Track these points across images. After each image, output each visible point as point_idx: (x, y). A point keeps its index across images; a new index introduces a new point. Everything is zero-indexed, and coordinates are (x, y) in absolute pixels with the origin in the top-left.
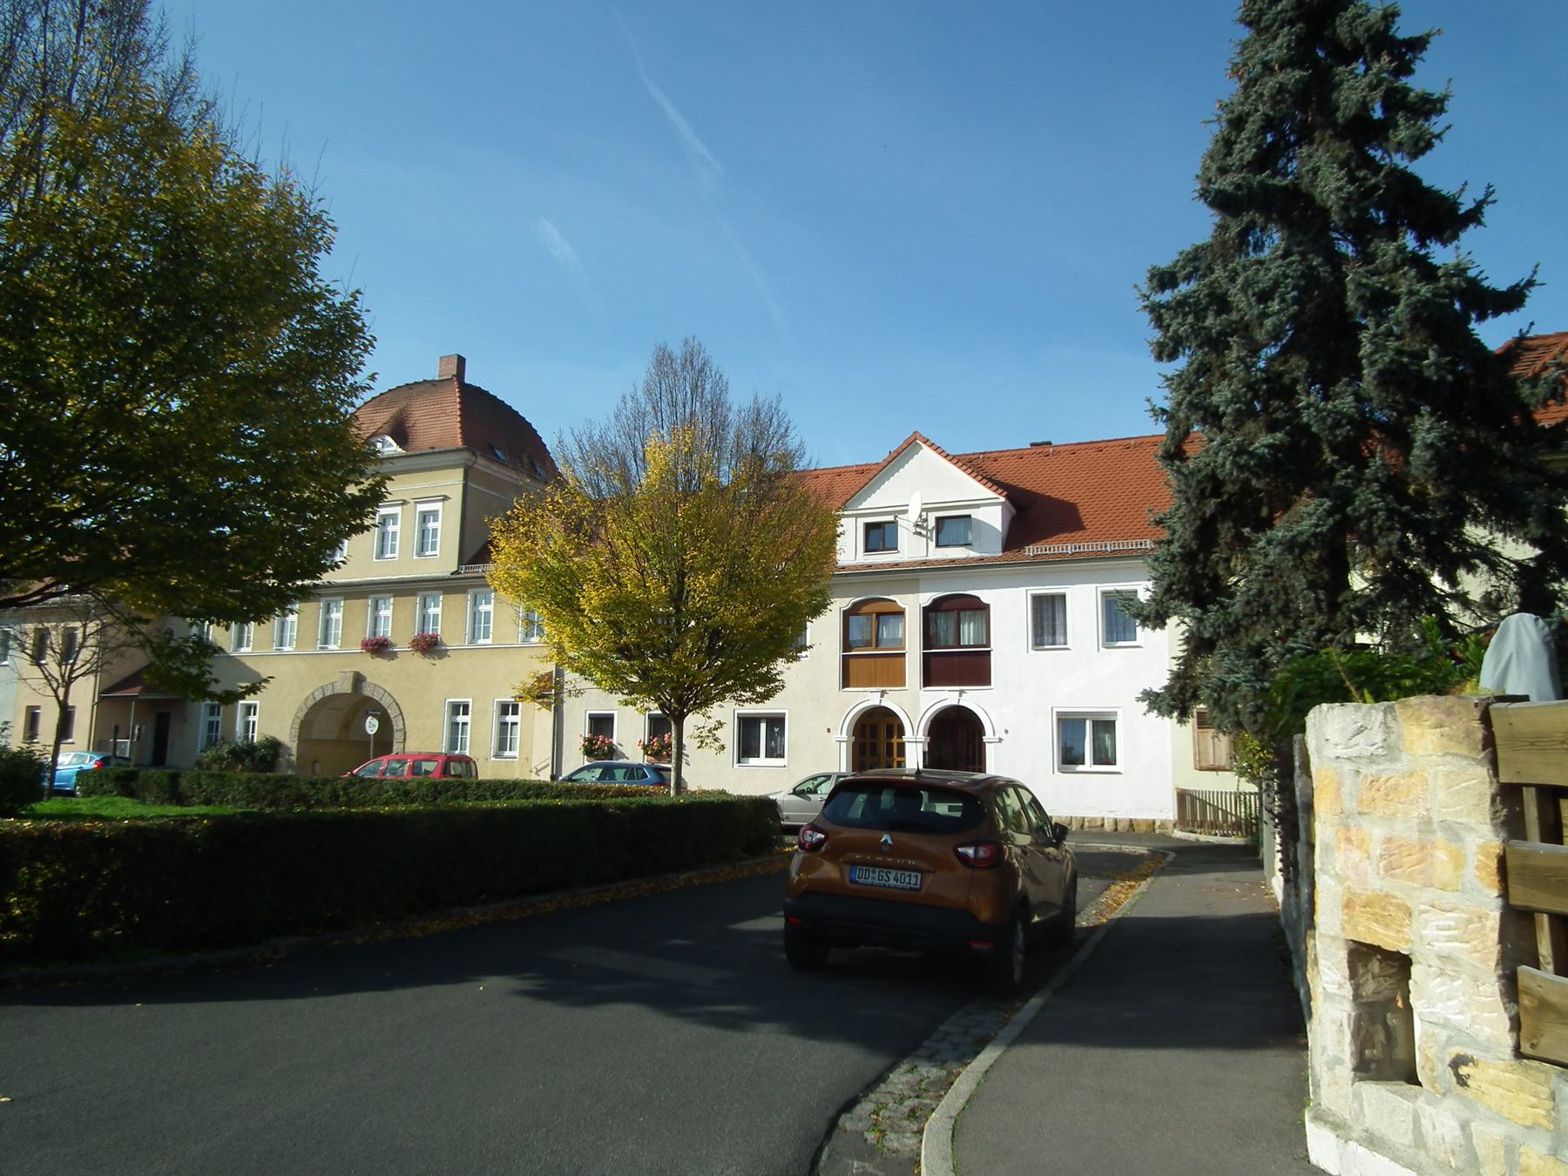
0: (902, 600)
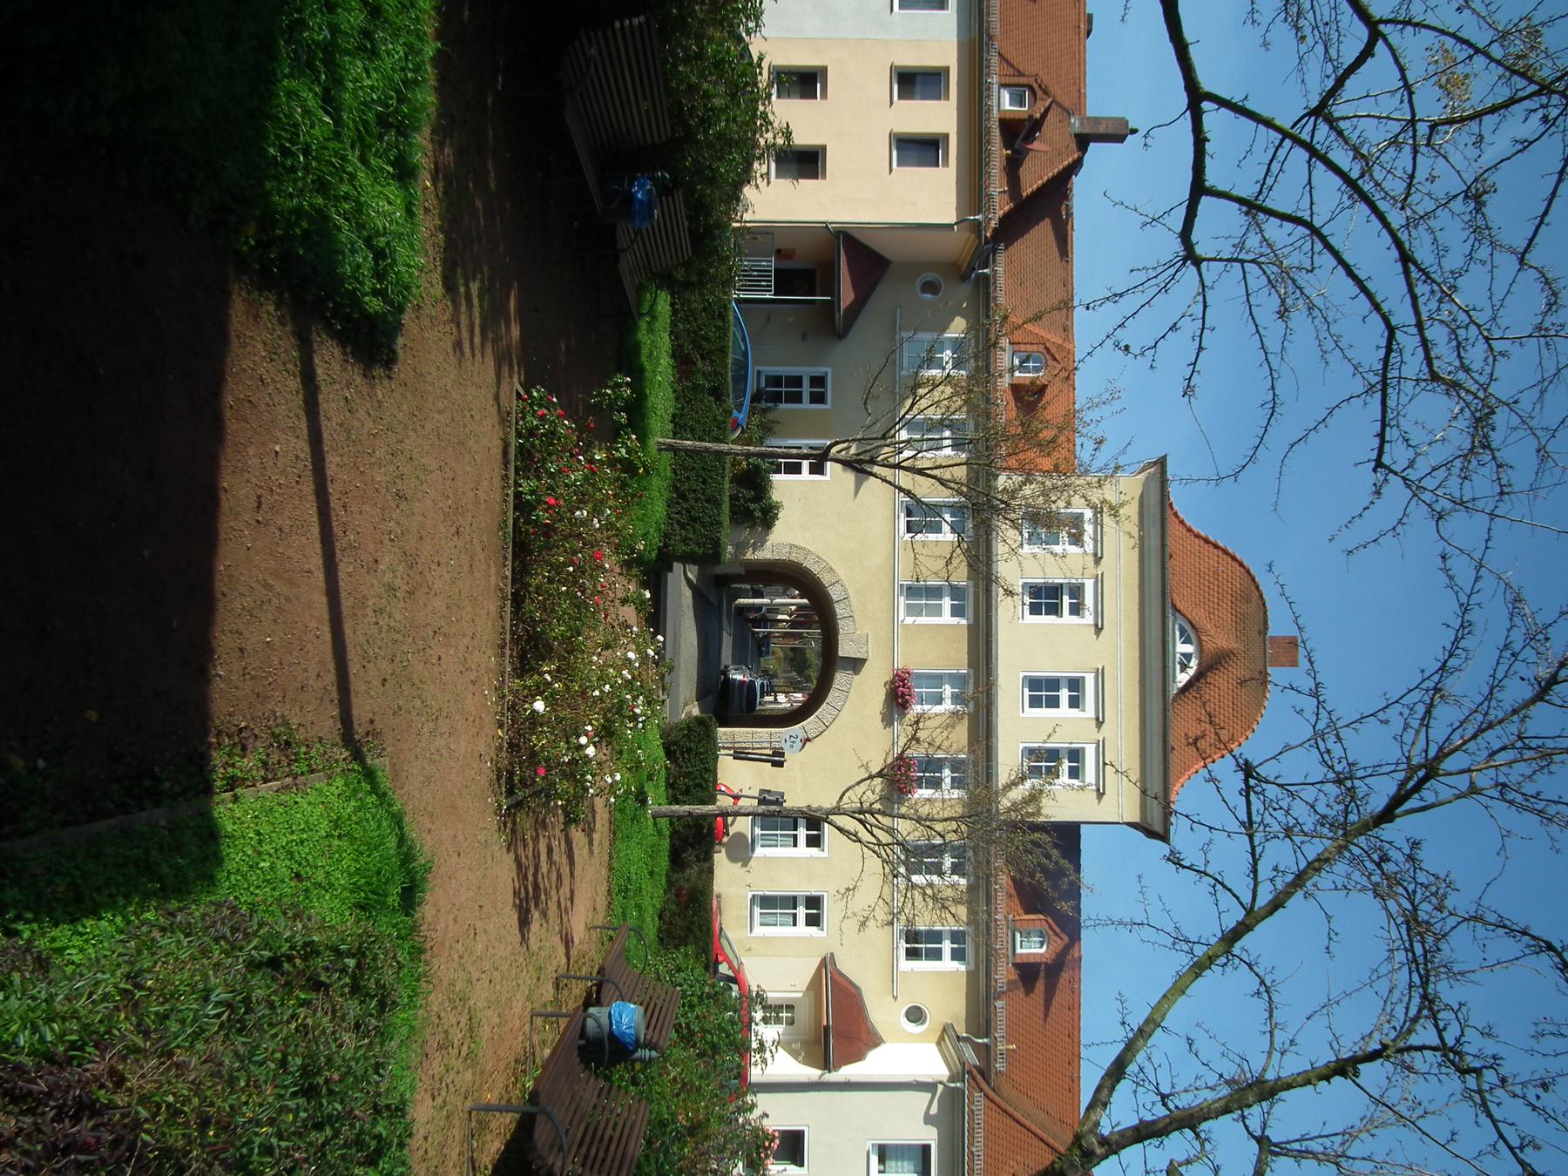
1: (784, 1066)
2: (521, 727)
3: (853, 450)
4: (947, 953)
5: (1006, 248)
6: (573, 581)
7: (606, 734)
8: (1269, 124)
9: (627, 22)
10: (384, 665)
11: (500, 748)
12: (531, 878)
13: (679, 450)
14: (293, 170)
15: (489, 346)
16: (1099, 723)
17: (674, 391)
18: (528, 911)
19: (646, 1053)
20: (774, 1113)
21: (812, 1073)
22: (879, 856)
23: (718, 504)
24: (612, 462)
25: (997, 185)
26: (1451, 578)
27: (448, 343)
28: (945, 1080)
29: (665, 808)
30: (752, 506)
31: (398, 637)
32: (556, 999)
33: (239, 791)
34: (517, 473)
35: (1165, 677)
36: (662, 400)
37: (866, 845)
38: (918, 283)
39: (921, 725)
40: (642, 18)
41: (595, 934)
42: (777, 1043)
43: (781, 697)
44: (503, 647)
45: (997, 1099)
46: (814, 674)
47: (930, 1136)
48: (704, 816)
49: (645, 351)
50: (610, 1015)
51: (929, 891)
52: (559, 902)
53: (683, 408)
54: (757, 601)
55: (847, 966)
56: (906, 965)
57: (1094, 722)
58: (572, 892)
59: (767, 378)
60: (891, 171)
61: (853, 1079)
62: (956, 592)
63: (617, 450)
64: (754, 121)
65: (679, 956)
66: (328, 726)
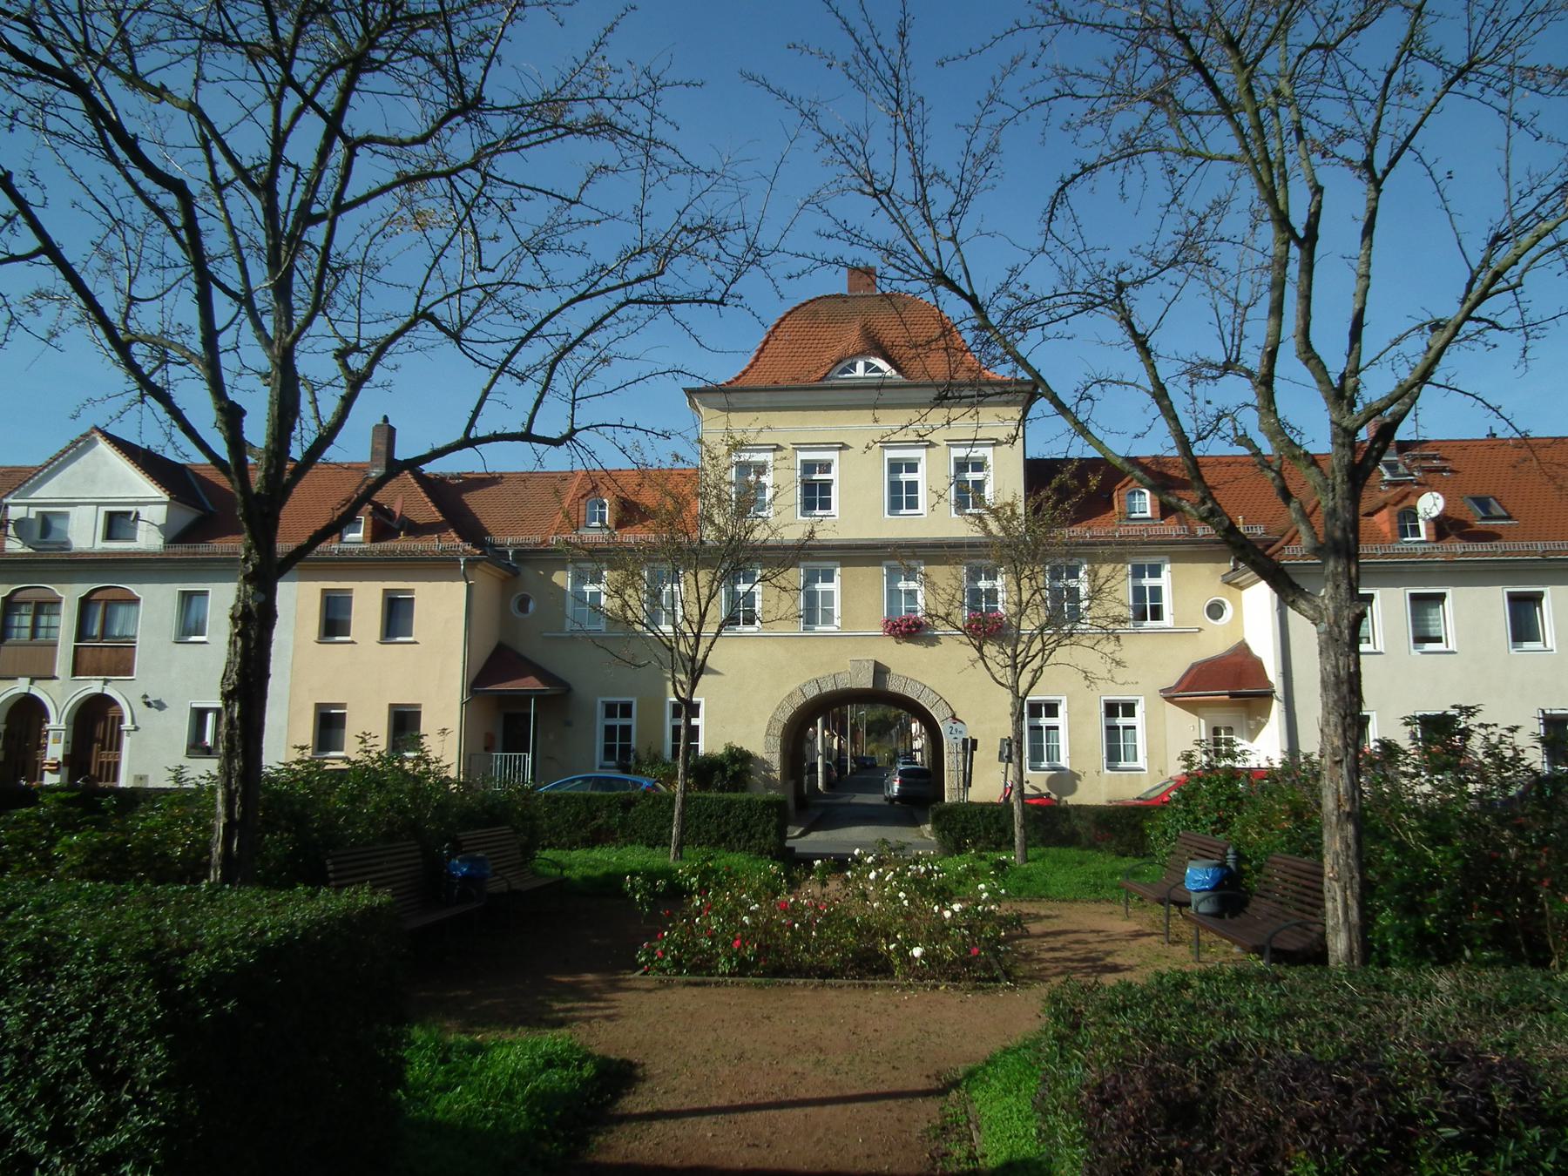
0: (58, 590)
2: (938, 970)
3: (682, 677)
4: (1154, 582)
5: (489, 534)
6: (806, 927)
7: (944, 895)
10: (881, 1069)
11: (956, 988)
12: (1075, 964)
13: (681, 840)
14: (499, 1116)
15: (605, 996)
17: (625, 845)
18: (1105, 966)
21: (1277, 708)
23: (731, 804)
24: (703, 891)
25: (431, 544)
29: (1018, 851)
30: (729, 773)
31: (858, 1059)
33: (978, 1153)
34: (713, 975)
36: (635, 856)
37: (1044, 661)
39: (933, 612)
40: (328, 862)
43: (917, 744)
44: (866, 986)
46: (893, 712)
48: (1025, 813)
49: (590, 872)
53: (641, 837)
55: (1172, 676)
56: (1168, 620)
59: (606, 759)
60: (415, 643)
61: (1280, 669)
62: (811, 579)
63: (691, 885)
64: (363, 778)
66: (932, 1105)
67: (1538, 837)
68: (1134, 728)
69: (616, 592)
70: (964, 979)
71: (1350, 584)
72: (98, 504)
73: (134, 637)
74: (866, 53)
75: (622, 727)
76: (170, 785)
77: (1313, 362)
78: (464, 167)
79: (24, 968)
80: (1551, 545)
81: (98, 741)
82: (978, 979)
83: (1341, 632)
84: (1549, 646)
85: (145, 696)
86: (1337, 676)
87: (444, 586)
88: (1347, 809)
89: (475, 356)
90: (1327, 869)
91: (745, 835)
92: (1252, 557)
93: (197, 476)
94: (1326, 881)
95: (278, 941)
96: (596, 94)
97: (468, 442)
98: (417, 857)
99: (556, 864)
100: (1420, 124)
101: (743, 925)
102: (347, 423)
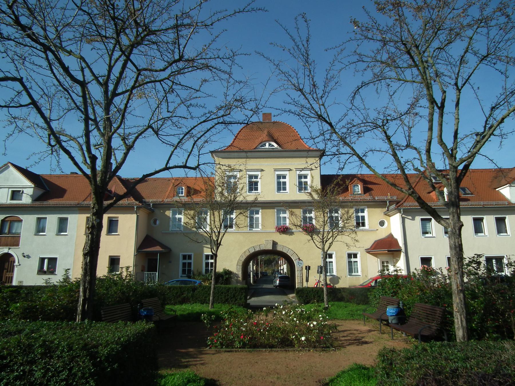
1: (401, 264)
2: (310, 345)
5: (144, 198)
7: (309, 319)
8: (173, 152)
9: (103, 316)
10: (300, 379)
11: (316, 351)
12: (353, 341)
15: (199, 356)
16: (290, 170)
17: (193, 303)
19: (401, 305)
20: (416, 266)
21: (403, 255)
22: (336, 237)
26: (279, 115)
27: (202, 366)
28: (401, 214)
30: (225, 278)
31: (291, 376)
32: (388, 333)
35: (274, 151)
38: (154, 225)
39: (296, 224)
40: (102, 311)
41: (367, 323)
42: (394, 266)
45: (405, 199)
47: (418, 219)
48: (327, 291)
49: (182, 313)
50: (391, 316)
51: (345, 222)
52: (359, 334)
53: (199, 301)
54: (251, 276)
55: (368, 245)
56: (367, 227)
57: (290, 172)
58: (355, 330)
60: (118, 235)
61: (403, 242)
65: (371, 297)
67: (509, 296)
68: (357, 262)
69: (192, 218)
70: (318, 347)
71: (458, 216)
72: (9, 188)
73: (20, 233)
74: (298, 46)
75: (188, 263)
76: (45, 285)
77: (443, 145)
78: (165, 79)
79: (42, 354)
80: (486, 203)
81: (5, 269)
82: (323, 347)
83: (456, 231)
84: (486, 234)
85: (23, 254)
86: (455, 245)
87: (128, 216)
88: (460, 288)
89: (162, 140)
90: (455, 308)
91: (234, 299)
92: (426, 207)
93: (43, 178)
94: (454, 313)
95: (126, 342)
96: (216, 57)
97: (167, 168)
98: (129, 309)
99: (172, 310)
100: (473, 73)
101: (242, 331)
102: (126, 161)
